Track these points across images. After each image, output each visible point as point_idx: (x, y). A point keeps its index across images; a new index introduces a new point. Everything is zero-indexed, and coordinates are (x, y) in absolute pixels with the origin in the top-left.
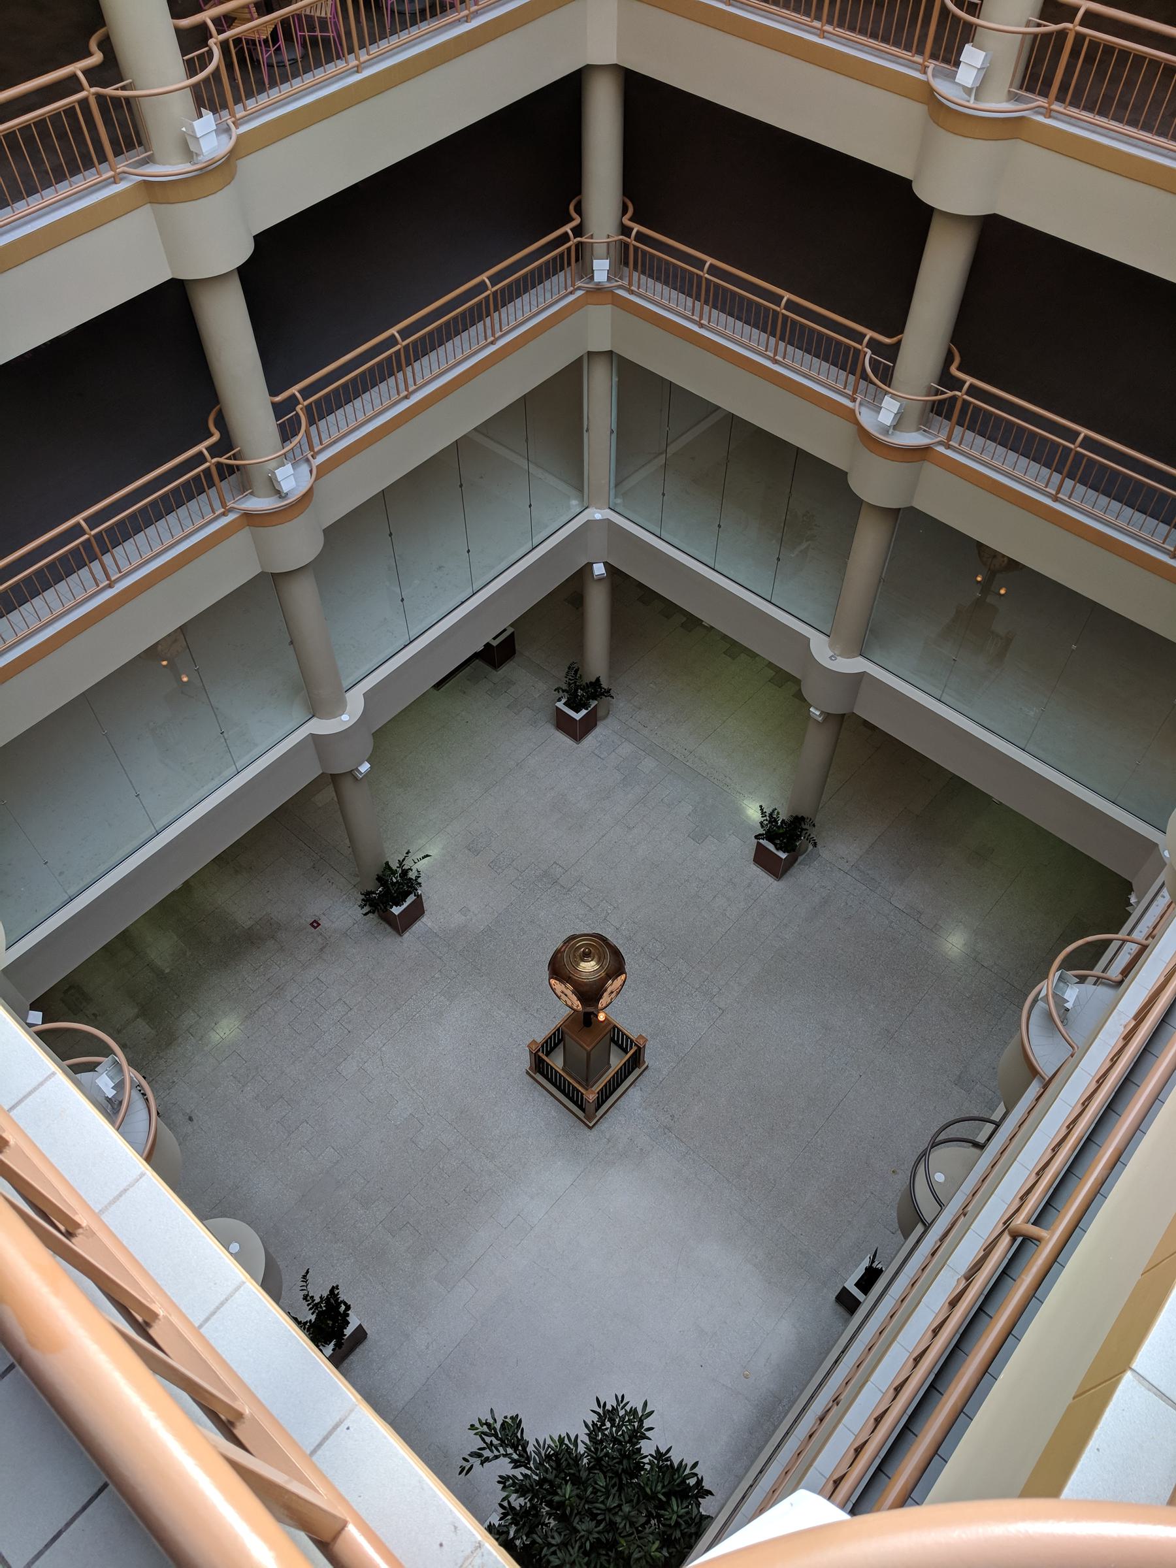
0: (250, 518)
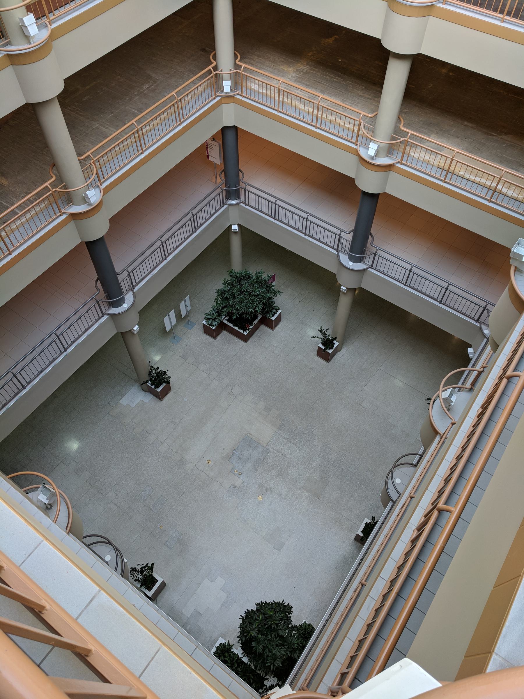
0: (74, 216)
